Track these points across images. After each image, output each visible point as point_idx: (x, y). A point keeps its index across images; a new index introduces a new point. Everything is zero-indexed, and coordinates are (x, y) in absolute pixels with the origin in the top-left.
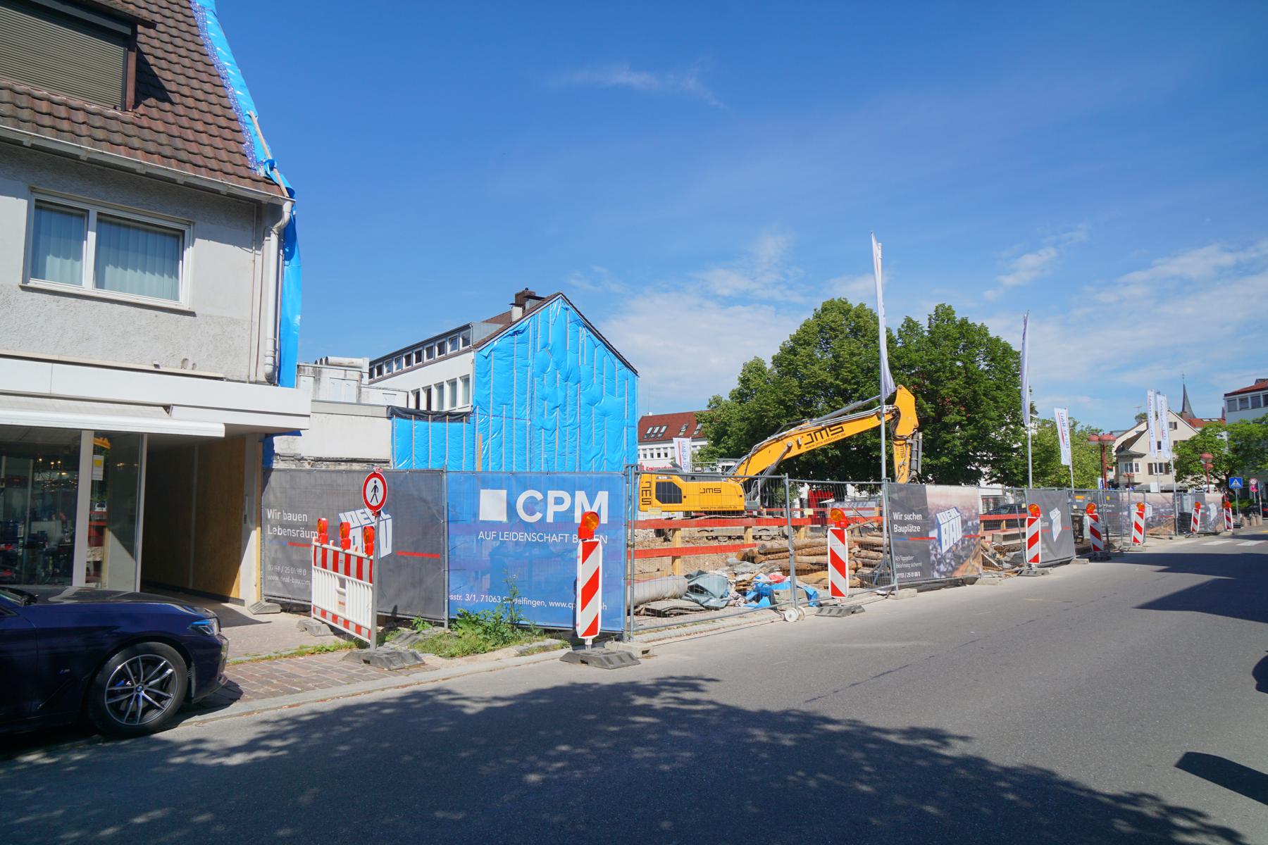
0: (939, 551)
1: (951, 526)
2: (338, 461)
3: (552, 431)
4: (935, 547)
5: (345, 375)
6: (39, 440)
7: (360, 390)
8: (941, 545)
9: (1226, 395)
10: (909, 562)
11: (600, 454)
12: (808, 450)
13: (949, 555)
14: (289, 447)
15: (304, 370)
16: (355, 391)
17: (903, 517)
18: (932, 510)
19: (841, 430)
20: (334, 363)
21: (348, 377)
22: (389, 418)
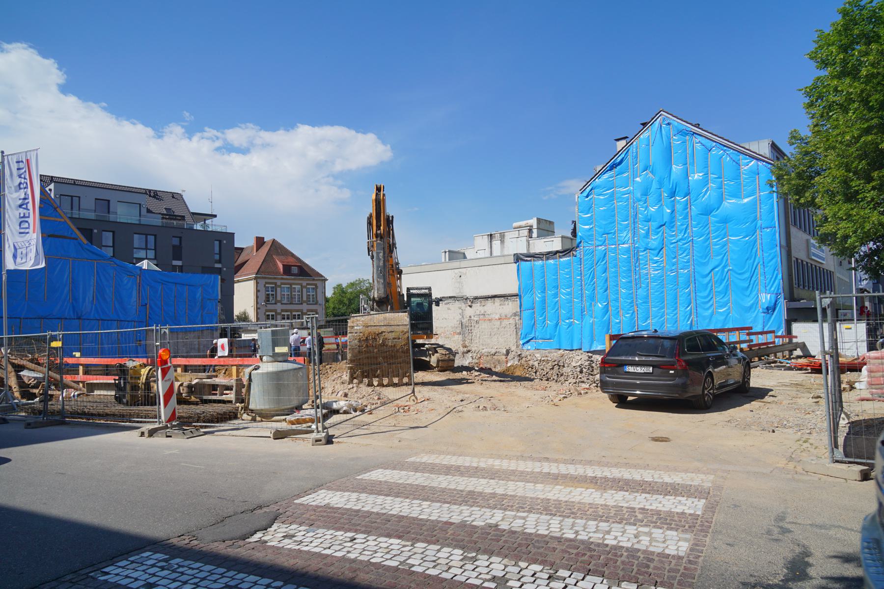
2: (486, 298)
3: (658, 251)
7: (529, 243)
9: (96, 199)
11: (722, 266)
16: (525, 244)
21: (521, 235)
22: (516, 263)
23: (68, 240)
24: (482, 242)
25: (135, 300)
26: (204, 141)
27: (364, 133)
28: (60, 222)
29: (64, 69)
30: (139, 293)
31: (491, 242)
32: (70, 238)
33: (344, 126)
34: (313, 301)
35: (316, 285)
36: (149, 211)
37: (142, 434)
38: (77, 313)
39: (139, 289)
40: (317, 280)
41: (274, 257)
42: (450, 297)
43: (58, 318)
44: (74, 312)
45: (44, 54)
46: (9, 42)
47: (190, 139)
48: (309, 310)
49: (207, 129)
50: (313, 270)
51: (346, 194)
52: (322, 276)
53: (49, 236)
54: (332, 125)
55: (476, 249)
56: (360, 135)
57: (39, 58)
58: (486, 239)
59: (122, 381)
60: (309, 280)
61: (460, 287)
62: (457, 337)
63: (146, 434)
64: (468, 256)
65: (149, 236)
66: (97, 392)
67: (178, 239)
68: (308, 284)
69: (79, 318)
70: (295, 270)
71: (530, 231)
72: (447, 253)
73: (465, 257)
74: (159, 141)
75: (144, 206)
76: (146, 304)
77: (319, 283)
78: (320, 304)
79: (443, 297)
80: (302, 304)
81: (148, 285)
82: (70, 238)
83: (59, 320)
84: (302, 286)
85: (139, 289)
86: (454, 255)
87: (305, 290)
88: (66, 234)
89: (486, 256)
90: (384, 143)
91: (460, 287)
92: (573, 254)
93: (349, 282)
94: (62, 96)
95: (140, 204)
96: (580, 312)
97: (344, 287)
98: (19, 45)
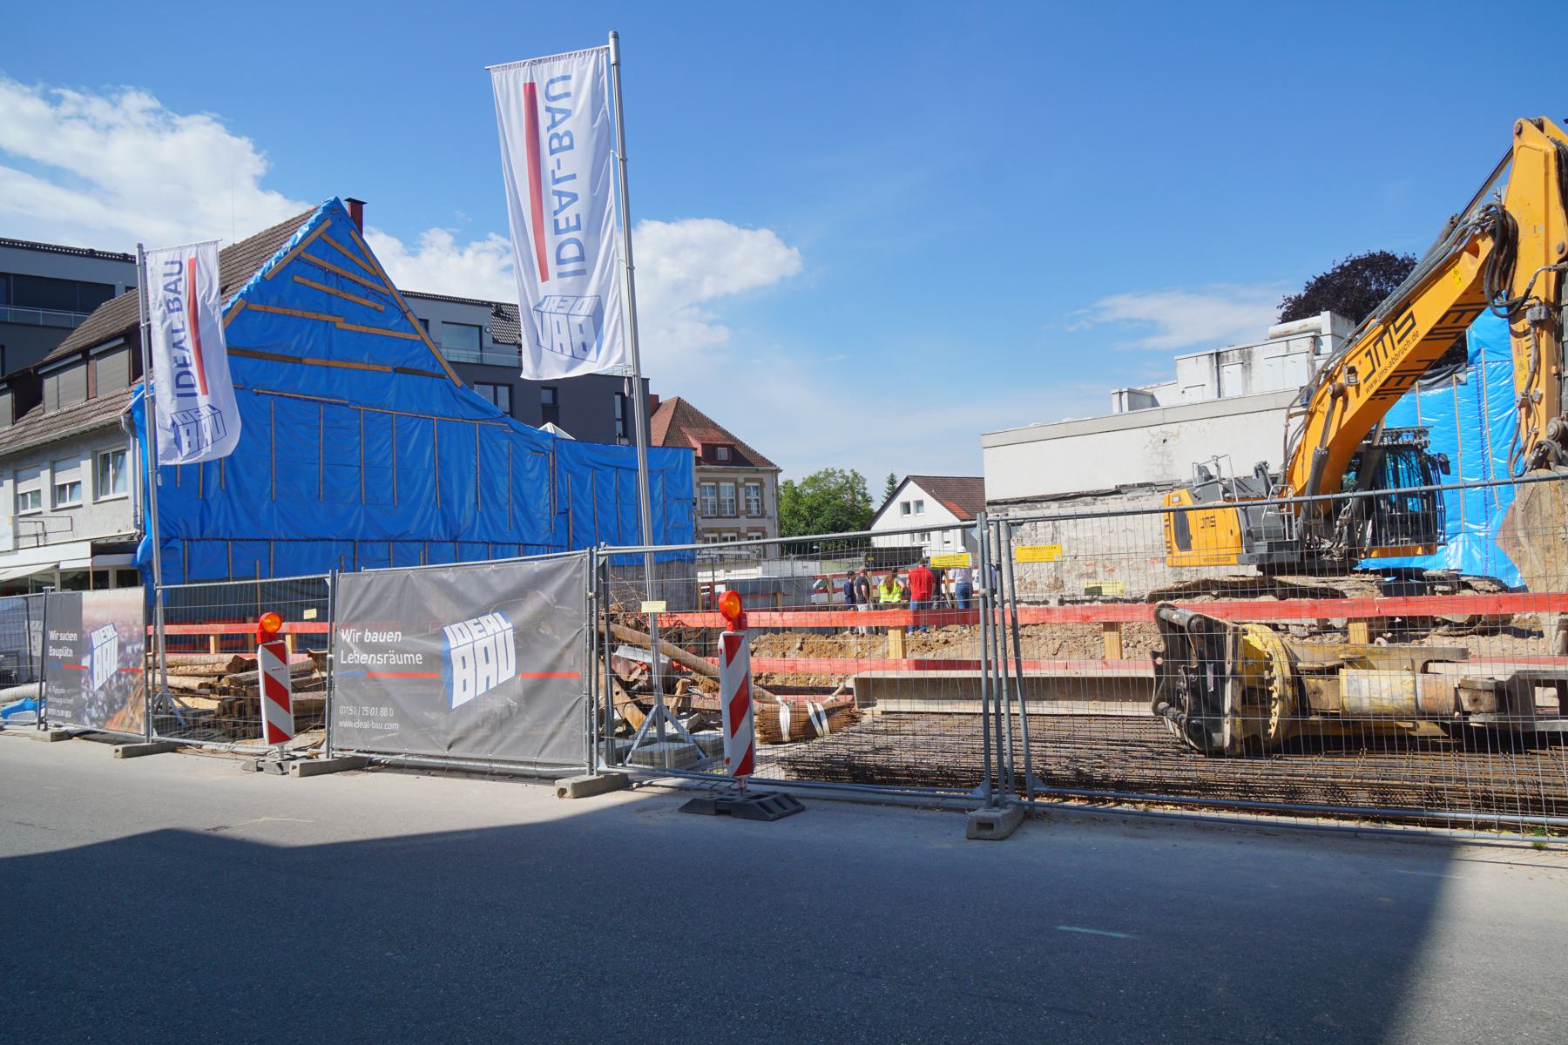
0: (91, 686)
1: (104, 652)
4: (86, 681)
5: (1288, 349)
6: (17, 583)
8: (92, 677)
10: (62, 696)
12: (1372, 391)
13: (102, 695)
14: (1165, 473)
15: (1227, 357)
17: (59, 637)
18: (87, 627)
19: (1410, 322)
20: (1278, 334)
21: (1292, 351)
23: (429, 380)
24: (1196, 370)
25: (547, 501)
26: (483, 256)
27: (754, 228)
28: (413, 341)
29: (265, 152)
30: (554, 488)
31: (1218, 368)
32: (433, 375)
33: (718, 219)
34: (758, 512)
35: (761, 481)
36: (495, 341)
37: (562, 792)
38: (451, 532)
39: (554, 479)
40: (763, 471)
41: (684, 429)
42: (1140, 486)
43: (418, 541)
44: (445, 529)
45: (235, 130)
46: (184, 114)
47: (461, 254)
48: (751, 529)
49: (492, 235)
50: (754, 453)
51: (722, 335)
52: (771, 464)
53: (396, 371)
54: (700, 217)
55: (1181, 387)
56: (746, 234)
57: (227, 137)
58: (1205, 365)
59: (1210, 676)
60: (748, 471)
61: (1165, 462)
62: (1159, 566)
63: (569, 793)
64: (1163, 400)
65: (499, 388)
66: (882, 705)
67: (549, 393)
68: (747, 480)
69: (454, 540)
70: (723, 453)
71: (1316, 340)
72: (1125, 396)
73: (1154, 403)
74: (411, 259)
75: (488, 330)
76: (567, 510)
77: (766, 478)
78: (769, 518)
79: (1122, 486)
80: (738, 517)
81: (570, 472)
82: (433, 375)
83: (420, 545)
84: (736, 483)
85: (554, 479)
86: (1140, 400)
87: (741, 491)
88: (424, 367)
89: (1209, 399)
90: (788, 242)
91: (1165, 462)
92: (1458, 381)
93: (806, 477)
94: (260, 194)
95: (480, 327)
96: (1481, 504)
97: (796, 485)
98: (198, 118)
